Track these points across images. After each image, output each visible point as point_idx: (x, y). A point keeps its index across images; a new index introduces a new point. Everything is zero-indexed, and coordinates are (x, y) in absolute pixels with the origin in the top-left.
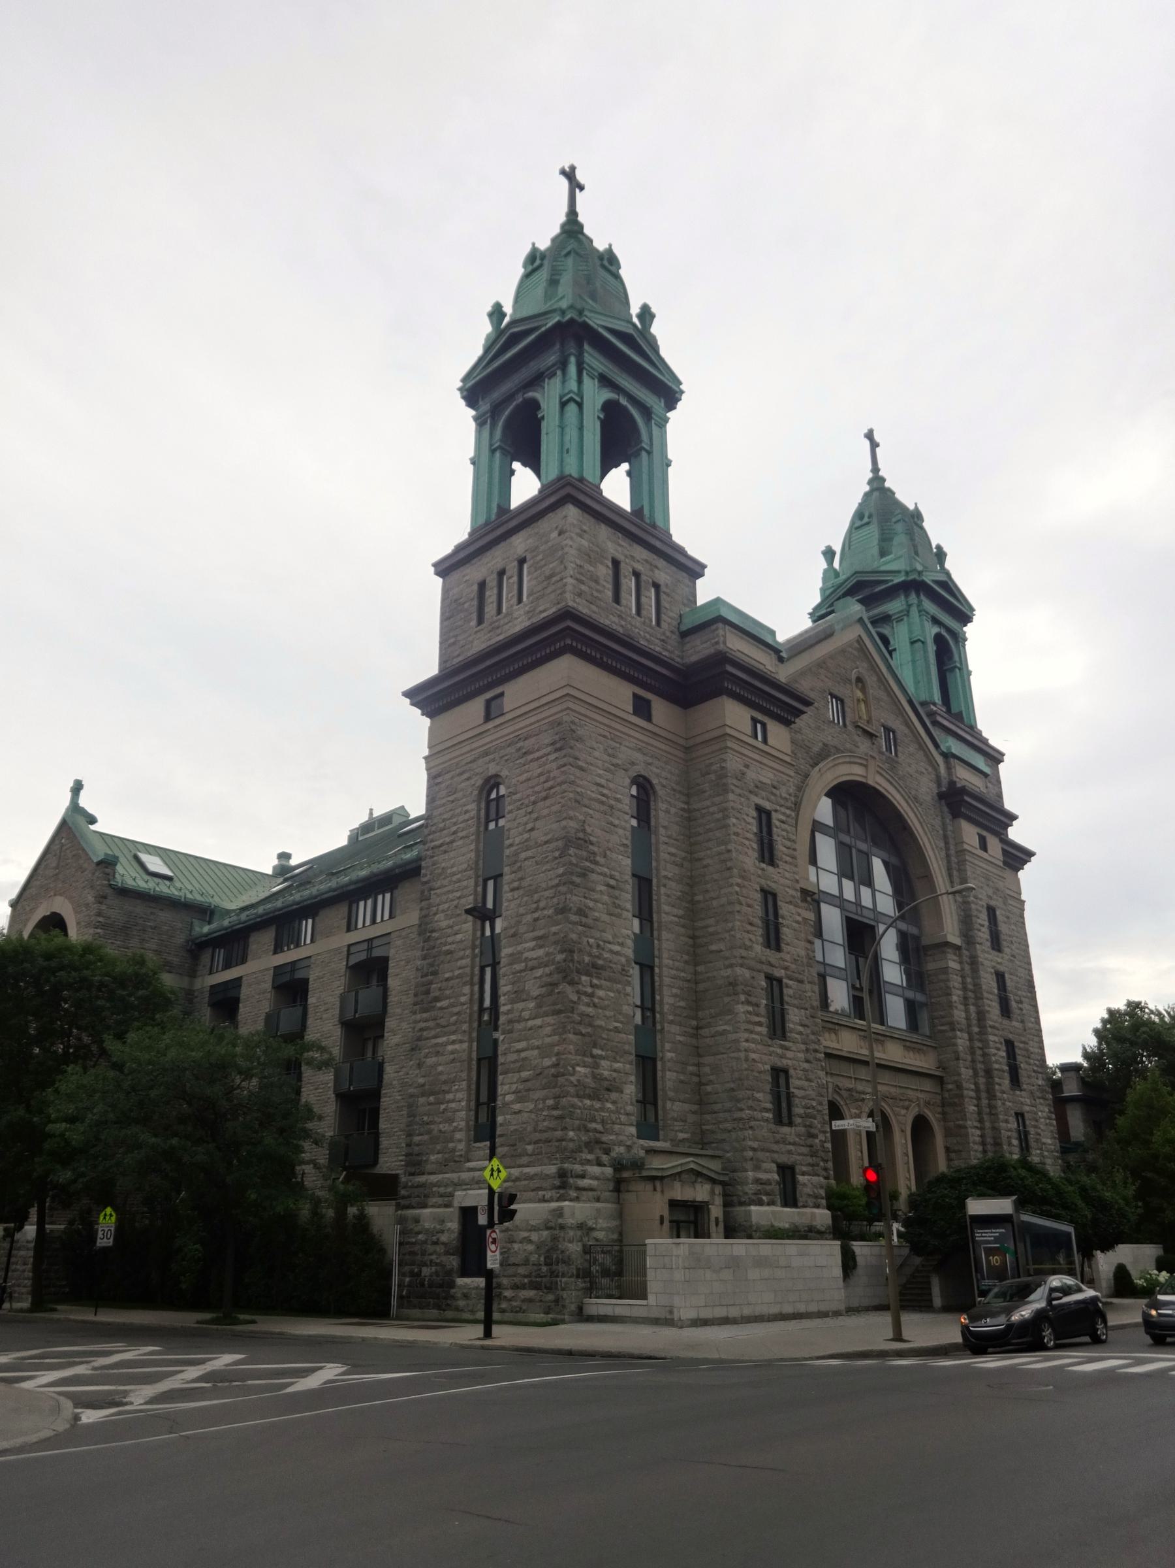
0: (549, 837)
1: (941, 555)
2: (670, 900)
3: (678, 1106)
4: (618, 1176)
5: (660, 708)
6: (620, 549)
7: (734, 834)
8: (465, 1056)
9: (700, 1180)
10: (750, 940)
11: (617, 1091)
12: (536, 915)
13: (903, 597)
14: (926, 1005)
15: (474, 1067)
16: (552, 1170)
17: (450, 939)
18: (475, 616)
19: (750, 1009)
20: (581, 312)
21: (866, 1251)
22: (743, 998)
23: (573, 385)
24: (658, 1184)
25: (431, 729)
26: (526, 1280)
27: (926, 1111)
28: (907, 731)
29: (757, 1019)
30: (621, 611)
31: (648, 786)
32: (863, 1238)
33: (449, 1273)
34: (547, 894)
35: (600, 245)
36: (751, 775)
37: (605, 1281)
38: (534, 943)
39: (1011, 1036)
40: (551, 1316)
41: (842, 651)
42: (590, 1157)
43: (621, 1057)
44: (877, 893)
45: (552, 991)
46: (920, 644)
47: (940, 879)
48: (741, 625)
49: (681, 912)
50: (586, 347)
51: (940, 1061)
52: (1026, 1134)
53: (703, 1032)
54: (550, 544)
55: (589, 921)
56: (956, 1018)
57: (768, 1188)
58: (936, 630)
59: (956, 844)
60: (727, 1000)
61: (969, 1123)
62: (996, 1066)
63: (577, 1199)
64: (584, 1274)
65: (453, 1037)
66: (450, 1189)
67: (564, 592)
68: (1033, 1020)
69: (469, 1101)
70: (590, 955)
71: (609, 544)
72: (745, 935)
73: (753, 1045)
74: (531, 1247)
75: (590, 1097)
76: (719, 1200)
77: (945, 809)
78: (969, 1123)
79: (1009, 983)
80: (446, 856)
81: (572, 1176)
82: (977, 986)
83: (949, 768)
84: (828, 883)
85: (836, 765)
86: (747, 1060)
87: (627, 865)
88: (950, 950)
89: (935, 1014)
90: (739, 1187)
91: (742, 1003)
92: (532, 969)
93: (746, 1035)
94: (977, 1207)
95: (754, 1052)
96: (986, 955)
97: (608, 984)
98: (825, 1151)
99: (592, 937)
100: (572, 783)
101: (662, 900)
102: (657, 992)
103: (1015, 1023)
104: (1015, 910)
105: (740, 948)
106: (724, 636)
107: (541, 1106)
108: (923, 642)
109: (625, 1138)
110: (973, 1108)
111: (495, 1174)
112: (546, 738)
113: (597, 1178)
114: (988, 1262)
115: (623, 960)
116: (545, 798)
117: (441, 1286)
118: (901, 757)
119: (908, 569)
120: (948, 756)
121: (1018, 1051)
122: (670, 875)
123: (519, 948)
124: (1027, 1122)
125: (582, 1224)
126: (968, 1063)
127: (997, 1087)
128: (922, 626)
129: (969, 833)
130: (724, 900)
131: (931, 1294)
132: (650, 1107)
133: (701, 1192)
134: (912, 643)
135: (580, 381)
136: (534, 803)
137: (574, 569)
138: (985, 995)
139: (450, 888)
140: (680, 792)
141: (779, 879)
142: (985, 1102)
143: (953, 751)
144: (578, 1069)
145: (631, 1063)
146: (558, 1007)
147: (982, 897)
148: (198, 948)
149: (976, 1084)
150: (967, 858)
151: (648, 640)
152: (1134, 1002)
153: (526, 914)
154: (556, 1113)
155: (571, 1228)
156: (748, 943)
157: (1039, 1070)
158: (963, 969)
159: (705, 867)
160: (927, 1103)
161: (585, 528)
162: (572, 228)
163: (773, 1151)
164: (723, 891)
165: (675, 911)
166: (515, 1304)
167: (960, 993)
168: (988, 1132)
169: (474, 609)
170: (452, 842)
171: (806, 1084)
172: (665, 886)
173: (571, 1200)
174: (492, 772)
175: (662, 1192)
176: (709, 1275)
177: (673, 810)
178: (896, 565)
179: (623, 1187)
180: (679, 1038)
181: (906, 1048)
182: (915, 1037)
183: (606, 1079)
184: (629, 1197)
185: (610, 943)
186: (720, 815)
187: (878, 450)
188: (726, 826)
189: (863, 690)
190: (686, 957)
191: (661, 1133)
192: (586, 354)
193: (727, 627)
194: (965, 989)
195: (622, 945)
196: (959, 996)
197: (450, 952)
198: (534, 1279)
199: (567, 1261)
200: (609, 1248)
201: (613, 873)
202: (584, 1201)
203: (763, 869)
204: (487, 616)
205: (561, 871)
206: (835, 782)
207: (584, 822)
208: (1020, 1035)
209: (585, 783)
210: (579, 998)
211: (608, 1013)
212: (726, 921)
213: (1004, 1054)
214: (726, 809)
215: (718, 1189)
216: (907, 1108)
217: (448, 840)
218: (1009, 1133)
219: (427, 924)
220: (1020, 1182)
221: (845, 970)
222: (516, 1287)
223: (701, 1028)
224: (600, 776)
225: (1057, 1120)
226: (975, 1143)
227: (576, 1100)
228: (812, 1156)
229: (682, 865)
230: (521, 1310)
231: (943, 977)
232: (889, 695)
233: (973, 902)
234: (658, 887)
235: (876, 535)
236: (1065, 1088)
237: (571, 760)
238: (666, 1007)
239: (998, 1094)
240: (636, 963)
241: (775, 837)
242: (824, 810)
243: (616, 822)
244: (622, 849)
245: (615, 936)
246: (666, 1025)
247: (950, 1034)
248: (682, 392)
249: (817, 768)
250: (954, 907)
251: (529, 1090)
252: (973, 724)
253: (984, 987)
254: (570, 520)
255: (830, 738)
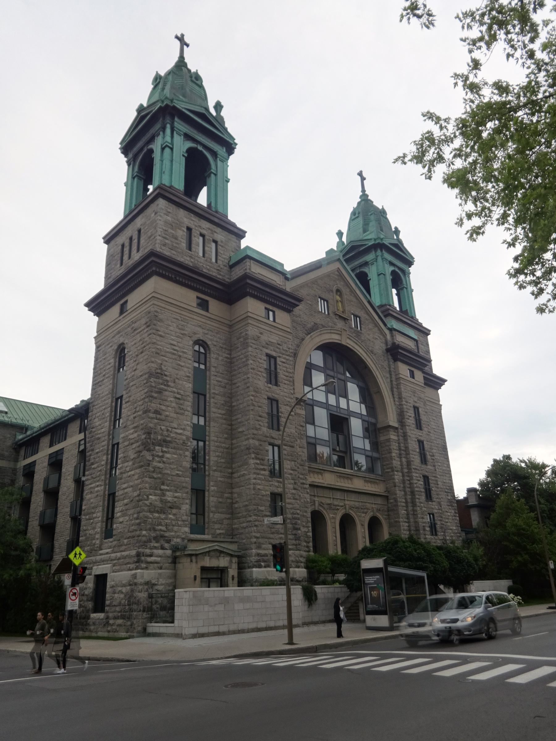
0: (142, 373)
1: (397, 232)
2: (216, 405)
3: (217, 516)
4: (174, 555)
5: (214, 305)
6: (192, 222)
7: (251, 369)
8: (102, 493)
9: (222, 555)
10: (260, 425)
11: (176, 509)
12: (135, 415)
13: (374, 252)
14: (380, 459)
15: (106, 499)
16: (133, 552)
17: (99, 432)
18: (119, 262)
19: (258, 462)
20: (172, 101)
21: (325, 590)
22: (253, 456)
23: (168, 139)
24: (194, 558)
25: (98, 323)
26: (119, 614)
27: (377, 514)
28: (367, 317)
29: (262, 467)
30: (192, 254)
31: (206, 346)
32: (324, 583)
33: (88, 611)
34: (140, 403)
35: (193, 70)
36: (264, 338)
37: (162, 613)
38: (133, 430)
39: (427, 474)
40: (129, 634)
41: (328, 275)
42: (156, 545)
43: (180, 490)
44: (350, 401)
45: (139, 455)
46: (382, 275)
47: (386, 393)
48: (260, 260)
49: (223, 412)
50: (176, 119)
51: (387, 488)
52: (435, 524)
53: (235, 475)
54: (151, 220)
55: (163, 417)
56: (394, 465)
57: (265, 558)
58: (392, 268)
59: (396, 375)
60: (245, 457)
61: (401, 520)
62: (416, 489)
63: (146, 568)
64: (148, 609)
65: (97, 484)
66: (91, 566)
67: (156, 244)
68: (445, 465)
69: (103, 517)
70: (162, 435)
71: (185, 219)
72: (257, 422)
73: (259, 481)
74: (122, 596)
75: (158, 512)
76: (235, 566)
77: (390, 357)
78: (401, 520)
79: (426, 446)
80: (100, 388)
81: (143, 556)
82: (407, 448)
83: (392, 336)
84: (320, 396)
85: (321, 334)
86: (254, 489)
87: (189, 387)
88: (391, 430)
89: (384, 463)
90: (248, 558)
91: (253, 458)
92: (132, 444)
93: (255, 476)
94: (366, 564)
95: (260, 485)
96: (412, 432)
97: (173, 450)
98: (308, 537)
99: (163, 426)
100: (154, 343)
101: (212, 406)
102: (207, 455)
103: (429, 467)
104: (436, 410)
105: (253, 429)
106: (250, 266)
107: (131, 518)
108: (384, 275)
109: (181, 534)
110: (404, 512)
111: (78, 556)
112: (143, 321)
113: (160, 556)
114: (371, 594)
115: (184, 437)
116: (142, 352)
117: (84, 618)
118: (364, 331)
119: (376, 237)
120: (391, 330)
121: (430, 481)
122: (217, 392)
123: (127, 433)
124: (436, 518)
125: (148, 582)
126: (401, 488)
127: (417, 500)
128: (384, 266)
129: (404, 369)
130: (245, 404)
131: (359, 613)
132: (201, 518)
133: (223, 562)
134: (379, 275)
135: (172, 137)
136: (137, 356)
137: (161, 232)
138: (411, 452)
139: (101, 405)
140: (225, 349)
141: (276, 392)
142: (410, 508)
143: (394, 327)
144: (150, 497)
145: (187, 493)
146: (142, 463)
147: (410, 400)
148: (18, 447)
149: (406, 499)
150: (402, 382)
151: (208, 269)
152: (506, 456)
153: (131, 415)
154: (137, 521)
155: (141, 584)
156: (258, 427)
157: (449, 491)
158: (399, 439)
159: (238, 387)
160: (378, 510)
161: (169, 210)
162: (181, 63)
163: (270, 538)
164: (245, 400)
165: (220, 411)
166: (114, 627)
167: (397, 452)
168: (412, 524)
169: (119, 259)
170: (103, 380)
171: (293, 501)
172: (213, 398)
173: (142, 569)
174: (121, 342)
175: (196, 562)
176: (206, 608)
177: (220, 358)
178: (371, 236)
179: (177, 560)
180: (219, 479)
181: (366, 481)
182: (372, 476)
183: (169, 502)
184: (179, 566)
185: (175, 428)
186: (244, 360)
187: (365, 181)
188: (247, 365)
189: (341, 296)
190: (226, 436)
191: (206, 530)
192: (175, 123)
193: (252, 261)
194: (400, 449)
195: (184, 429)
196: (396, 453)
197: (99, 438)
198: (122, 613)
199: (138, 603)
200: (166, 595)
201: (179, 391)
202: (152, 569)
203: (270, 388)
204: (124, 261)
205: (146, 391)
206: (321, 343)
207: (161, 364)
208: (433, 473)
209: (162, 343)
210: (153, 459)
211: (172, 466)
212: (246, 415)
213: (422, 483)
214: (247, 356)
215: (235, 560)
216: (366, 513)
217: (101, 379)
218: (424, 525)
219: (91, 424)
220: (404, 549)
221: (329, 441)
222: (115, 618)
223: (234, 473)
224: (173, 340)
225: (459, 517)
226: (404, 530)
227: (148, 514)
228: (296, 540)
229: (225, 387)
230: (116, 631)
231: (388, 444)
232: (357, 299)
233: (405, 404)
234: (209, 399)
235: (362, 222)
236: (469, 500)
237: (154, 331)
238: (212, 463)
239: (418, 504)
240: (193, 439)
241: (278, 371)
242: (318, 358)
243: (183, 364)
244: (186, 378)
245: (179, 425)
246: (211, 472)
247: (392, 473)
248: (236, 144)
249: (309, 336)
250: (394, 408)
251: (127, 510)
252: (414, 316)
253: (410, 448)
254: (160, 206)
255: (318, 320)
